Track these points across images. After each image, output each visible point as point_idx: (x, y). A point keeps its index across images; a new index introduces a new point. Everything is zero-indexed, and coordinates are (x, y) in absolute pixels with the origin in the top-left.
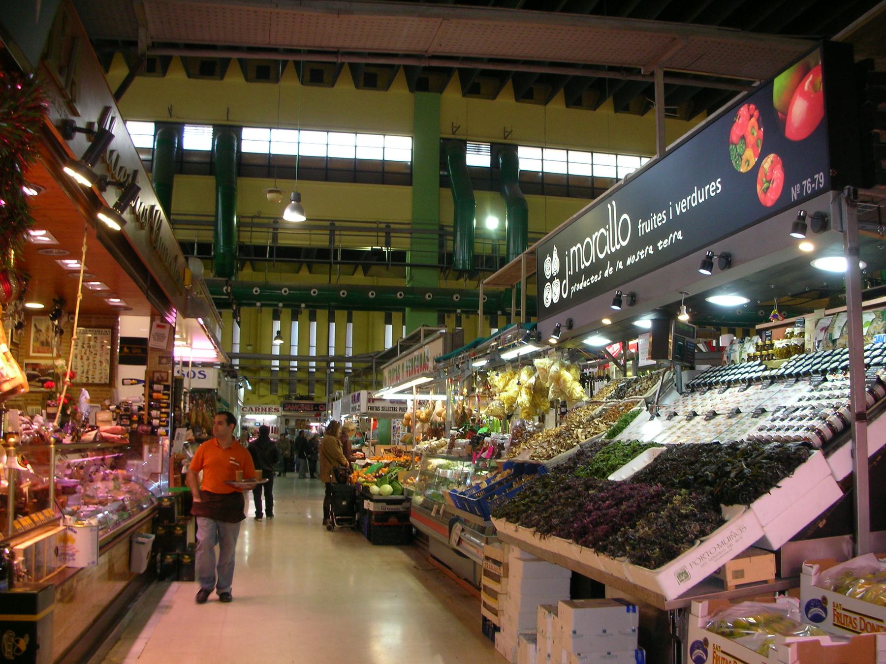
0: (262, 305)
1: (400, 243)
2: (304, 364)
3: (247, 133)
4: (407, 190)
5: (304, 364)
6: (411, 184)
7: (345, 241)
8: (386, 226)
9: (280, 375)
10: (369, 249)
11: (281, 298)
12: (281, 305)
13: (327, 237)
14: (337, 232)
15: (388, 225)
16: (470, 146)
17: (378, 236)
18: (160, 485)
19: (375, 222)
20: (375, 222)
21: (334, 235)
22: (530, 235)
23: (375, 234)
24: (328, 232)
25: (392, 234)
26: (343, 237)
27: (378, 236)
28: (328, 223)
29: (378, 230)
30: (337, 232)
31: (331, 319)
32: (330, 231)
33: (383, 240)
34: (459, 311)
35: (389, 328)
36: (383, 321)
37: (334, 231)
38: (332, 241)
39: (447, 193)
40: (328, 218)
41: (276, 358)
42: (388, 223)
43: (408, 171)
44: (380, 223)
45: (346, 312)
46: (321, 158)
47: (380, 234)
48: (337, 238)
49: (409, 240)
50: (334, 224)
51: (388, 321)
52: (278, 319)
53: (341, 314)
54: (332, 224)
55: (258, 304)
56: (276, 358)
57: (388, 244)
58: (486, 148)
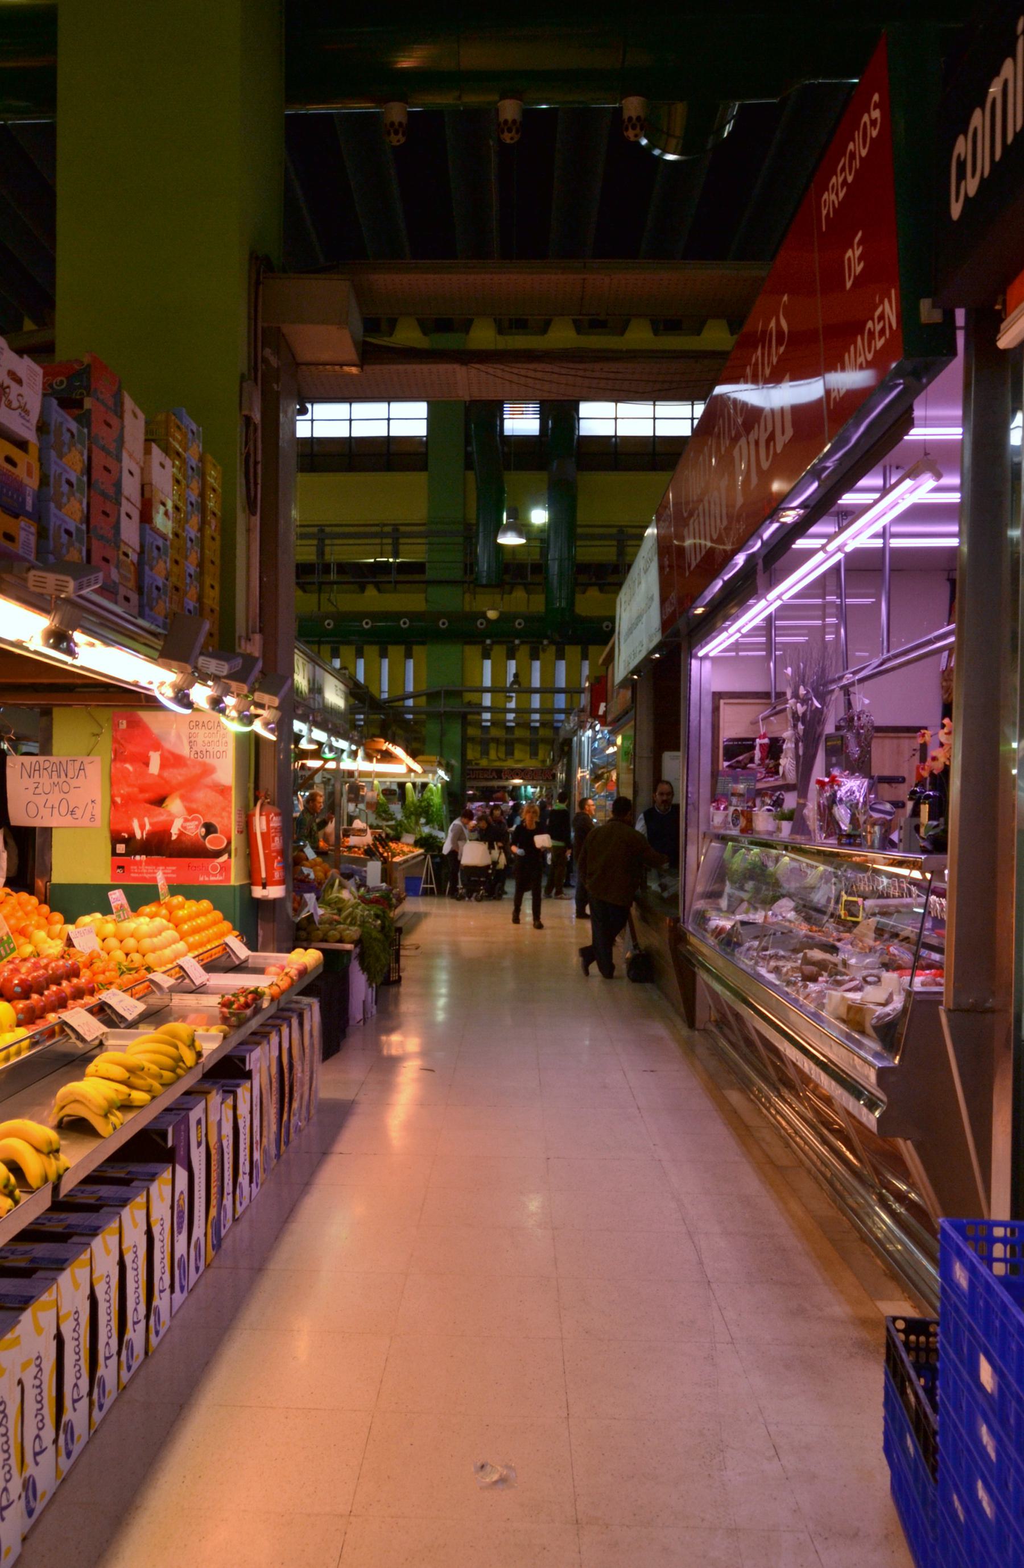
0: (493, 643)
1: (411, 553)
2: (500, 716)
3: (586, 409)
4: (420, 478)
5: (500, 716)
6: (424, 468)
7: (338, 553)
8: (393, 530)
9: (542, 732)
10: (372, 560)
11: (517, 634)
12: (517, 642)
13: (614, 550)
14: (327, 542)
15: (396, 527)
16: (507, 407)
17: (382, 544)
18: (850, 871)
19: (377, 525)
20: (377, 525)
21: (324, 545)
22: (579, 530)
23: (378, 541)
24: (315, 542)
25: (402, 541)
26: (335, 548)
27: (382, 544)
28: (614, 531)
29: (381, 535)
30: (327, 542)
31: (383, 654)
32: (319, 539)
33: (389, 548)
34: (488, 642)
35: (488, 664)
36: (329, 654)
37: (398, 539)
38: (321, 553)
39: (471, 475)
40: (316, 523)
41: (536, 711)
42: (621, 526)
43: (423, 450)
44: (385, 525)
45: (403, 647)
46: (608, 438)
47: (385, 541)
48: (327, 549)
49: (424, 548)
50: (397, 530)
51: (486, 655)
52: (489, 658)
53: (396, 651)
54: (322, 531)
55: (488, 642)
56: (536, 711)
57: (396, 555)
58: (533, 408)
